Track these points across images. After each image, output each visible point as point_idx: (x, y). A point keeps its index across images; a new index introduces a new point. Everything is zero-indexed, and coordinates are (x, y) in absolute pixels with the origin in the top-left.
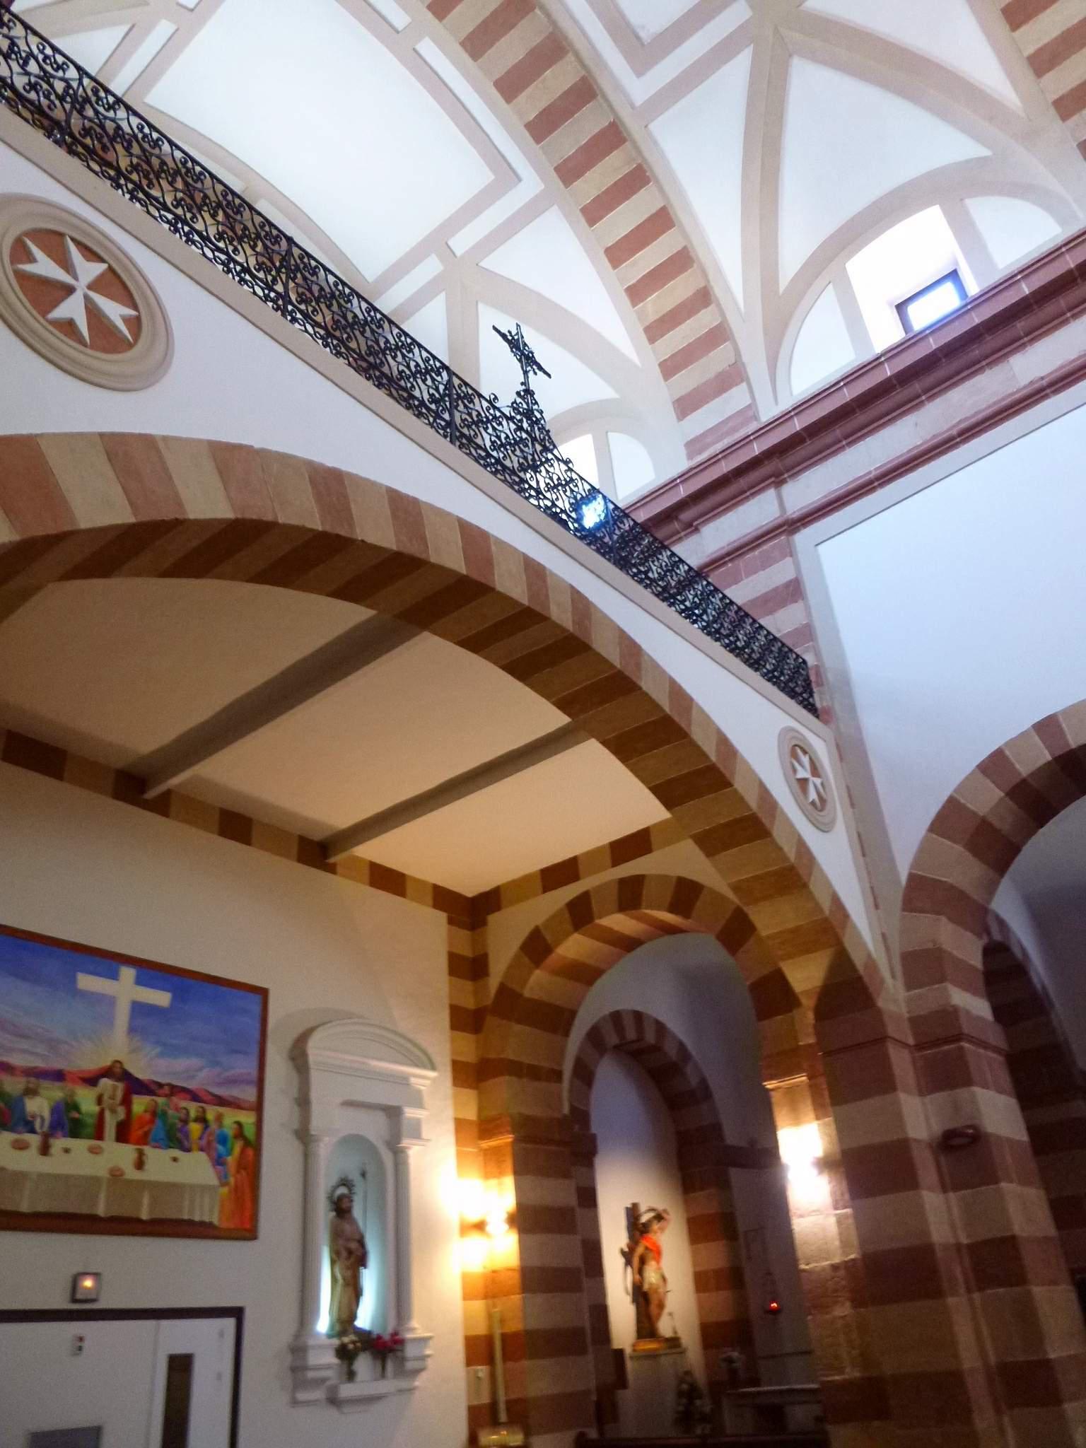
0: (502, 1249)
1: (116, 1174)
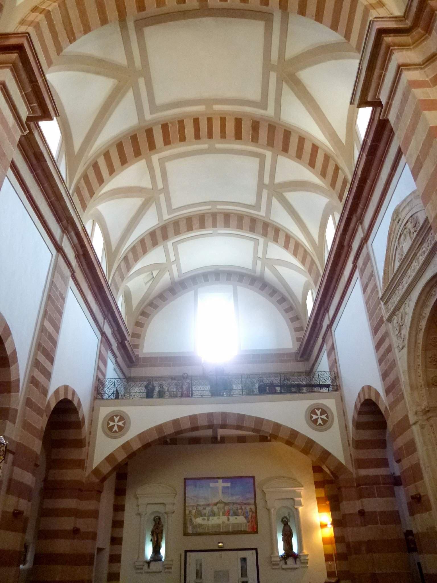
0: (329, 532)
1: (224, 523)
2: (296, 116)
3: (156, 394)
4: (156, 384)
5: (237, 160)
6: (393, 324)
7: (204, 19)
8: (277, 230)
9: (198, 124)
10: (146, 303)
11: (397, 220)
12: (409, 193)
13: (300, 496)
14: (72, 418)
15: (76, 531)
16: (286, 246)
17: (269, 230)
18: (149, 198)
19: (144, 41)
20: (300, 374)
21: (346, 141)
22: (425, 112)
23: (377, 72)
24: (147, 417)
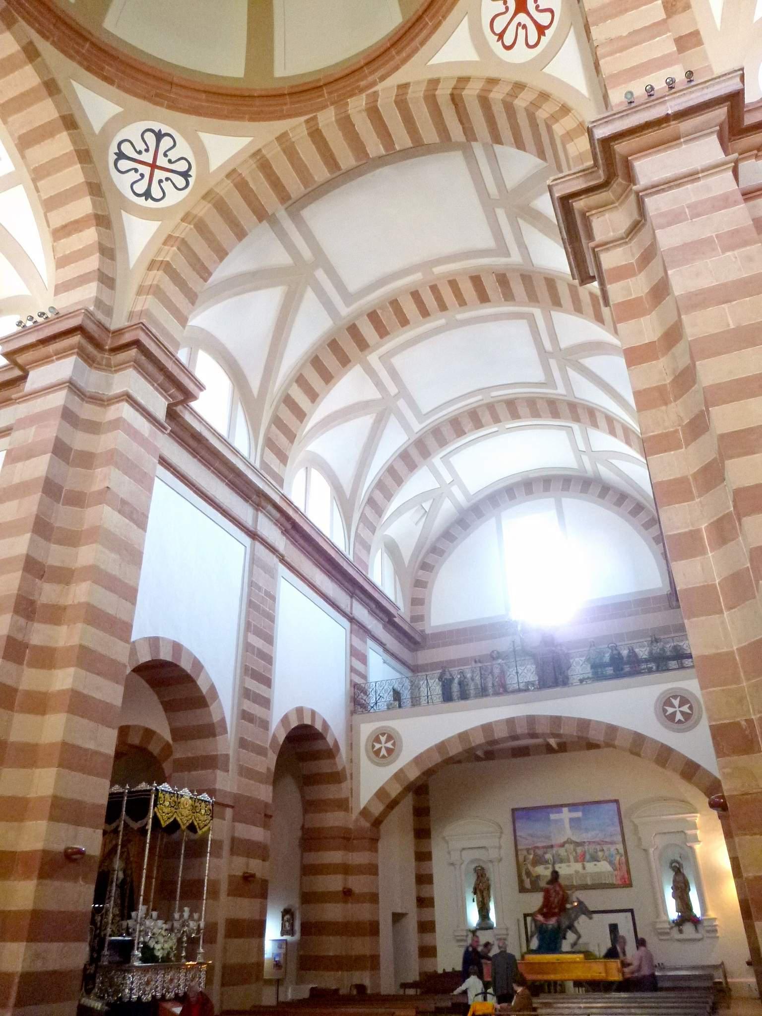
3: (423, 701)
4: (455, 671)
5: (495, 329)
7: (378, 171)
10: (424, 551)
13: (695, 827)
14: (318, 745)
15: (347, 893)
16: (612, 432)
19: (307, 226)
24: (427, 731)
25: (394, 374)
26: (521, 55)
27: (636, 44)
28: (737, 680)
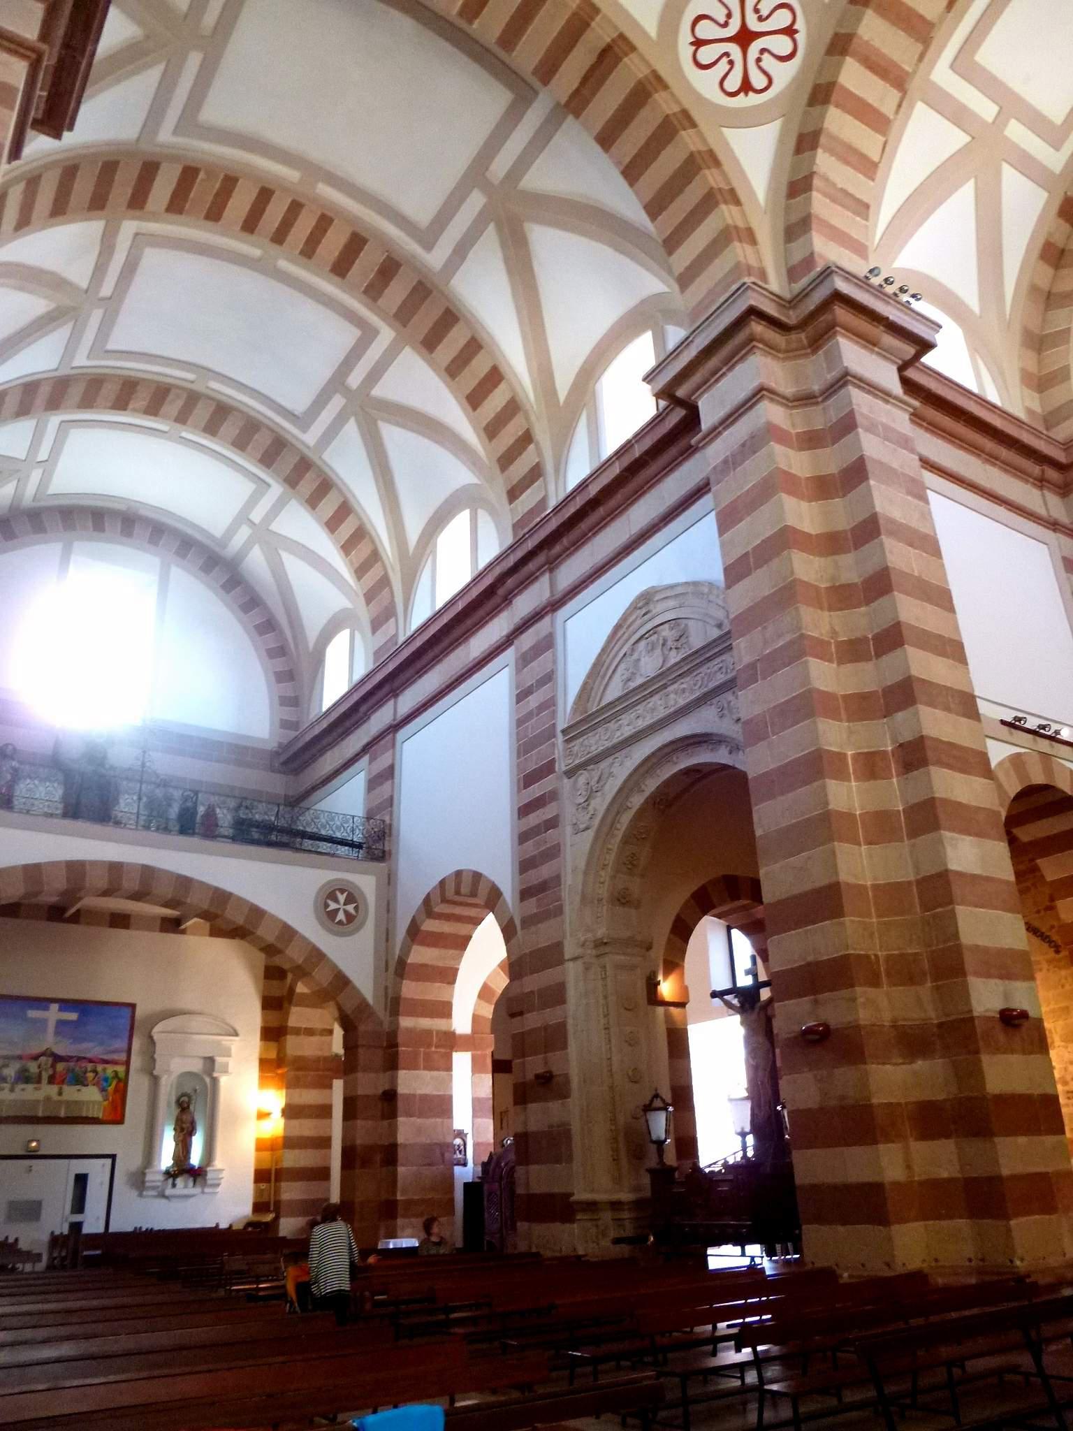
1: (48, 1099)
2: (485, 295)
5: (310, 312)
6: (576, 782)
8: (325, 486)
9: (268, 201)
11: (644, 611)
12: (684, 580)
16: (332, 525)
17: (307, 478)
18: (66, 306)
20: (272, 800)
21: (567, 398)
22: (784, 496)
23: (713, 362)
25: (130, 269)
26: (705, 84)
27: (843, 206)
28: (869, 916)
